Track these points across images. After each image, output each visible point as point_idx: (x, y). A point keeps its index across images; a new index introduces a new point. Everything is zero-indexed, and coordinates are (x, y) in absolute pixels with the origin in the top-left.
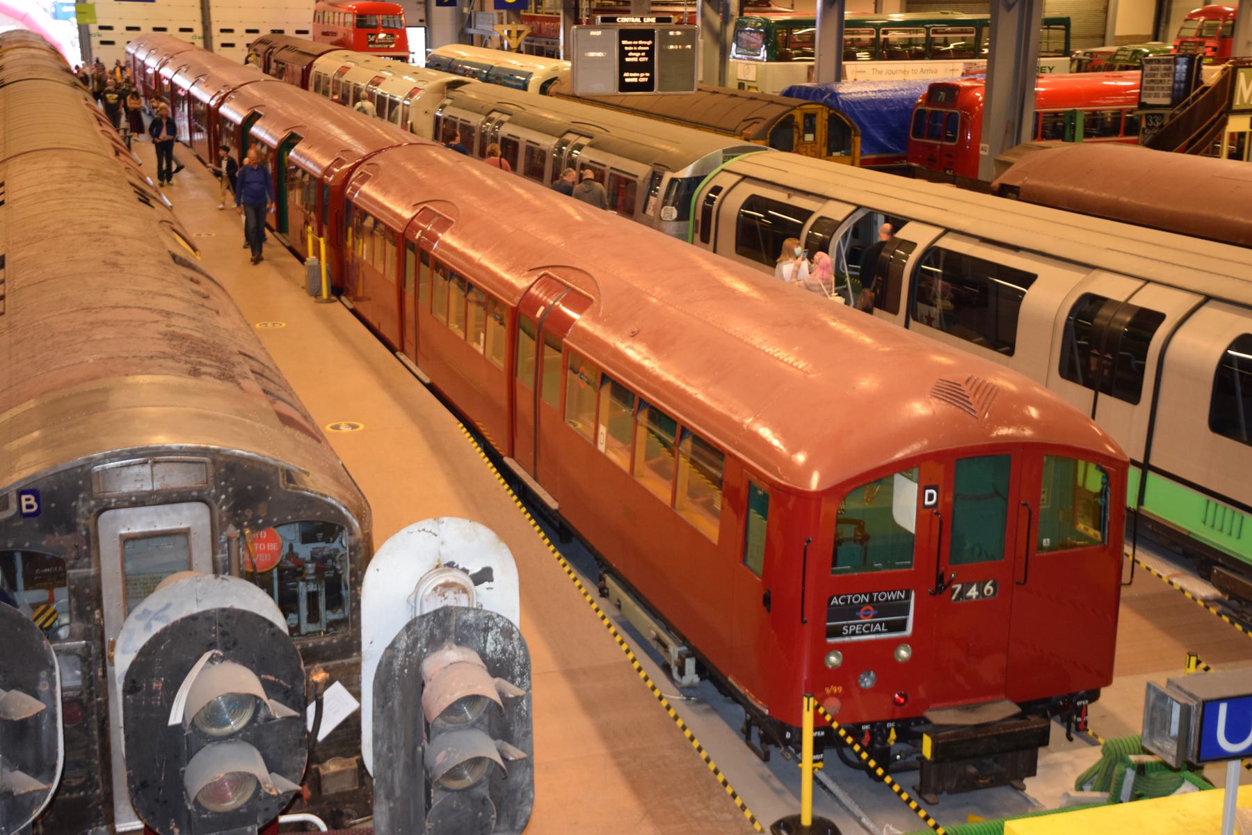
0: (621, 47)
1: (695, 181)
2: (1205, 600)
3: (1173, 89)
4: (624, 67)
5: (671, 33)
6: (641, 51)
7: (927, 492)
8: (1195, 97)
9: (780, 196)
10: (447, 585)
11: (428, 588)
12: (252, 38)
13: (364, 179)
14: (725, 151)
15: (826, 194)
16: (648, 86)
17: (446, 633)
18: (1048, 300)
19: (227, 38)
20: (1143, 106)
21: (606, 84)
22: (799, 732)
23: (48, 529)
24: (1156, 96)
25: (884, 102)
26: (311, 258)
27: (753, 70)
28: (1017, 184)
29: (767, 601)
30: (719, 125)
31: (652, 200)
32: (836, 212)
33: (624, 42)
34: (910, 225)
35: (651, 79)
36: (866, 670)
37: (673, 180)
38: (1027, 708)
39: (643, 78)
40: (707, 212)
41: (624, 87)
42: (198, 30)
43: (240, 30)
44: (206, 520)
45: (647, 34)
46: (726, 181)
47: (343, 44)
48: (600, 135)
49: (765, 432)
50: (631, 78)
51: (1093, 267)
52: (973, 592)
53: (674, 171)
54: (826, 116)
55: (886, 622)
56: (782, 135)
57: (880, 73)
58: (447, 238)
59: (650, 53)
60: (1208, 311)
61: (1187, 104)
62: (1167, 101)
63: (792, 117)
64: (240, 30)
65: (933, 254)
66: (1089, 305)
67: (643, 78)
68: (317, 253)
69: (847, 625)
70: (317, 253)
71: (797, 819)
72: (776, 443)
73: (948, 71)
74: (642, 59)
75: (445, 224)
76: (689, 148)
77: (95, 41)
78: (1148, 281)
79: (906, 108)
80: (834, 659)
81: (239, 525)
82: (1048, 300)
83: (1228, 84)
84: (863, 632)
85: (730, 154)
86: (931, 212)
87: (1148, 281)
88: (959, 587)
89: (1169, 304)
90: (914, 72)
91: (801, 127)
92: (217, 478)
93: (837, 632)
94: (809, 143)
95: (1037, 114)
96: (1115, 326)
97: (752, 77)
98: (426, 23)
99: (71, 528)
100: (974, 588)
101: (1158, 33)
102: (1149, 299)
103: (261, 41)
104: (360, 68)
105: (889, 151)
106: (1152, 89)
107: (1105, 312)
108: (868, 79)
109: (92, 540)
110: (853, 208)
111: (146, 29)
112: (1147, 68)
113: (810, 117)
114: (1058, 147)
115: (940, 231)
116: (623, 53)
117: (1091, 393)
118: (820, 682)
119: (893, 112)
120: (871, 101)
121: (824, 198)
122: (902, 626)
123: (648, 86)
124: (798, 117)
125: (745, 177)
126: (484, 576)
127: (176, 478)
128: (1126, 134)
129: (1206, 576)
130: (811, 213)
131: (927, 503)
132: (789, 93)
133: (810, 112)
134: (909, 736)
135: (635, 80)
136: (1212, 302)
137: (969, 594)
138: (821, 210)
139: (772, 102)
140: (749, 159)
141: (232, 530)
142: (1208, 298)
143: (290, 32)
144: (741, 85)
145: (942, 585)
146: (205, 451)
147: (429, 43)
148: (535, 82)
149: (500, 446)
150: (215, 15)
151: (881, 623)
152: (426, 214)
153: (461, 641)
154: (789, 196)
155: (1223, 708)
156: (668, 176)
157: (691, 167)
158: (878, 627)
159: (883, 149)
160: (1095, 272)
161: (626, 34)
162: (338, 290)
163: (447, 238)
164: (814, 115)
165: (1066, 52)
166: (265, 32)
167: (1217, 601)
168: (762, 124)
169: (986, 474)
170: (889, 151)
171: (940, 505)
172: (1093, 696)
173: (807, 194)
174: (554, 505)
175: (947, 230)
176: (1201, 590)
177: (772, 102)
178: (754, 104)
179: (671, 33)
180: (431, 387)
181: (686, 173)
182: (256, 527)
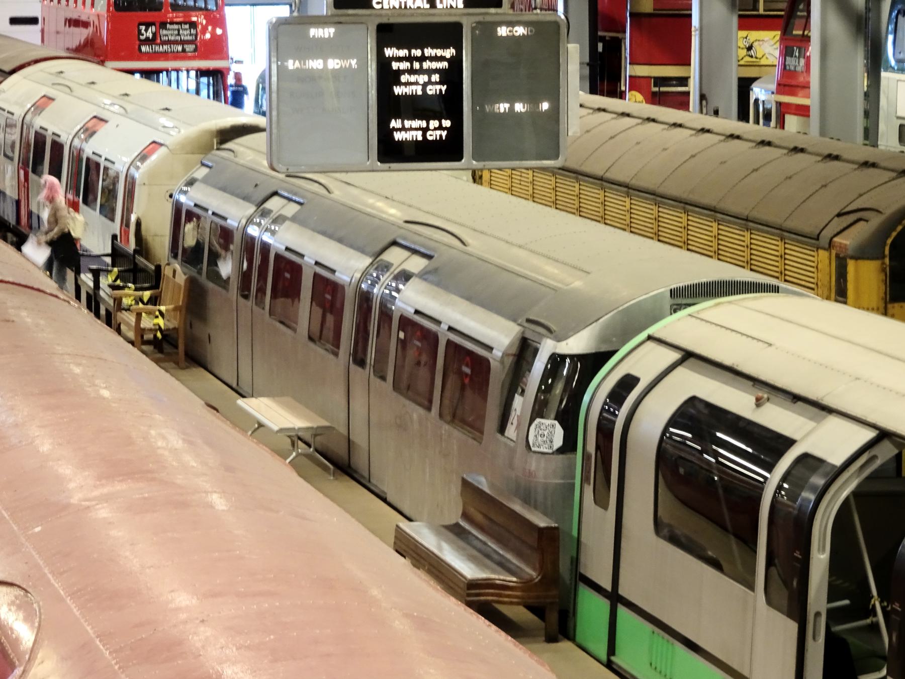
0: (384, 64)
1: (592, 363)
4: (390, 106)
5: (503, 31)
6: (430, 72)
14: (673, 293)
30: (789, 224)
32: (835, 442)
33: (389, 52)
37: (556, 361)
40: (605, 430)
46: (645, 361)
50: (408, 130)
53: (559, 339)
60: (680, 371)
74: (431, 90)
116: (387, 76)
125: (688, 356)
135: (419, 136)
154: (759, 403)
156: (547, 348)
168: (875, 221)
179: (503, 31)
181: (578, 343)
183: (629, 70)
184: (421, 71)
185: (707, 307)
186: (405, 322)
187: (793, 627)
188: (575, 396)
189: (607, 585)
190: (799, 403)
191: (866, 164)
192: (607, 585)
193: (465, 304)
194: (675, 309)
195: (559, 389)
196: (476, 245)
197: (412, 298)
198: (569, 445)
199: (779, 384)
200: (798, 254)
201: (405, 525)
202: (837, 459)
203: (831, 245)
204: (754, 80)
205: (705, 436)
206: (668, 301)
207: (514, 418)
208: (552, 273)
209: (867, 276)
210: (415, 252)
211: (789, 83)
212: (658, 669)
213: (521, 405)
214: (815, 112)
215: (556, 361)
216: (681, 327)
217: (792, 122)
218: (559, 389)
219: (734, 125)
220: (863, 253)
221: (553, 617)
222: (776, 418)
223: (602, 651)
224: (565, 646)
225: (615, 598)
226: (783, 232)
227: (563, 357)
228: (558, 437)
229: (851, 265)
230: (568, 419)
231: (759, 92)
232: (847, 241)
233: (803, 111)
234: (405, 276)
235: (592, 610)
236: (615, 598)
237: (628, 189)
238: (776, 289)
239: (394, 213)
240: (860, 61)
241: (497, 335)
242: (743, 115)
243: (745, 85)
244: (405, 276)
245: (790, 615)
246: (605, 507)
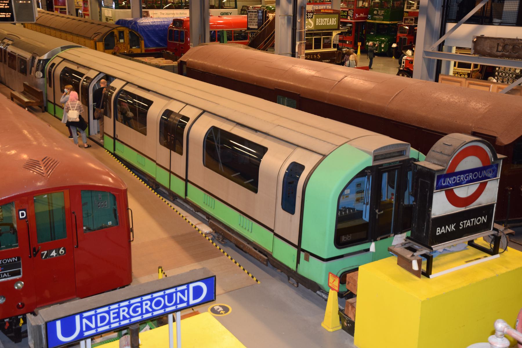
1: (47, 61)
2: (206, 234)
3: (258, 22)
6: (5, 3)
7: (20, 212)
8: (265, 25)
14: (61, 48)
15: (91, 67)
20: (249, 29)
24: (253, 25)
25: (157, 26)
27: (110, 12)
28: (185, 60)
30: (86, 36)
31: (33, 69)
32: (92, 74)
34: (116, 80)
35: (12, 15)
36: (18, 291)
37: (39, 61)
39: (8, 15)
40: (50, 73)
46: (57, 61)
49: (92, 166)
51: (172, 98)
52: (54, 254)
53: (40, 56)
54: (128, 32)
55: (9, 272)
57: (164, 14)
60: (63, 62)
61: (263, 27)
62: (256, 27)
63: (113, 33)
66: (168, 113)
67: (8, 15)
72: (97, 168)
73: (183, 14)
78: (187, 104)
79: (166, 29)
85: (63, 48)
87: (187, 104)
88: (46, 252)
89: (190, 113)
90: (177, 14)
91: (118, 36)
94: (121, 43)
95: (211, 31)
96: (175, 121)
97: (110, 15)
100: (54, 251)
105: (161, 46)
106: (251, 22)
110: (98, 73)
112: (249, 14)
114: (217, 45)
115: (125, 83)
117: (169, 150)
119: (161, 30)
121: (89, 68)
124: (116, 32)
125: (64, 59)
128: (234, 40)
131: (21, 217)
133: (121, 30)
135: (4, 16)
136: (206, 113)
137: (52, 254)
139: (106, 26)
140: (68, 52)
142: (204, 111)
144: (107, 19)
145: (36, 252)
151: (6, 273)
154: (78, 68)
155: (58, 324)
156: (38, 58)
157: (46, 55)
158: (5, 275)
159: (158, 45)
160: (172, 100)
164: (123, 32)
165: (236, 8)
167: (210, 233)
168: (101, 35)
170: (161, 46)
171: (28, 217)
173: (84, 67)
175: (128, 83)
176: (205, 229)
177: (106, 26)
181: (45, 57)
183: (54, 7)
184: (3, 3)
185: (67, 50)
186: (9, 53)
187: (87, 107)
188: (44, 68)
189: (53, 102)
190: (259, 133)
191: (99, 24)
192: (53, 102)
193: (21, 50)
194: (62, 51)
195: (41, 66)
196: (22, 38)
197: (10, 49)
198: (43, 77)
199: (82, 64)
200: (87, 41)
201: (13, 92)
202: (92, 77)
203: (93, 39)
204: (78, 9)
205: (168, 117)
206: (60, 49)
207: (32, 71)
208: (38, 44)
209: (100, 45)
210: (10, 40)
211: (85, 9)
212: (244, 227)
213: (34, 69)
214: (90, 15)
215: (39, 61)
216: (63, 54)
217: (87, 17)
218: (41, 66)
219: (74, 17)
220: (99, 41)
221: (43, 108)
222: (81, 70)
223: (53, 113)
224: (46, 113)
225: (55, 104)
226: (85, 37)
227: (41, 60)
228: (41, 75)
229: (97, 43)
230: (43, 71)
231: (80, 11)
232: (96, 38)
233: (88, 15)
234: (8, 45)
235: (51, 106)
236: (55, 104)
237: (54, 29)
238: (81, 47)
239: (6, 32)
240: (97, 6)
241: (28, 56)
242: (77, 16)
243: (77, 10)
244: (8, 45)
245: (86, 105)
246: (292, 212)
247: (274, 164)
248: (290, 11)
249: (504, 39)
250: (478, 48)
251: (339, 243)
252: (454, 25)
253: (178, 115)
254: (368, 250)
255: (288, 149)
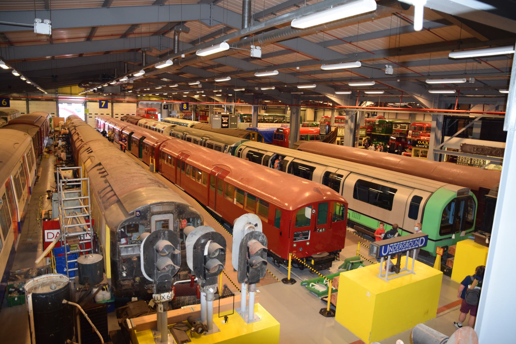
1: (235, 148)
4: (223, 123)
9: (256, 151)
10: (250, 227)
11: (247, 228)
12: (122, 116)
13: (164, 146)
16: (228, 127)
17: (252, 237)
18: (319, 172)
19: (117, 116)
20: (320, 134)
21: (218, 126)
22: (288, 261)
23: (141, 219)
25: (268, 132)
26: (151, 164)
29: (281, 234)
32: (270, 154)
38: (330, 253)
39: (226, 125)
41: (222, 127)
42: (111, 114)
43: (93, 114)
44: (172, 217)
45: (227, 116)
46: (243, 147)
47: (143, 117)
48: (211, 137)
50: (224, 125)
52: (321, 231)
56: (248, 137)
58: (188, 159)
59: (228, 120)
60: (351, 175)
64: (120, 114)
65: (293, 163)
66: (327, 174)
67: (226, 125)
68: (152, 162)
69: (297, 238)
70: (152, 162)
71: (287, 278)
75: (188, 156)
76: (234, 141)
77: (88, 117)
80: (295, 245)
81: (179, 219)
82: (319, 172)
83: (336, 130)
84: (300, 240)
85: (242, 142)
86: (291, 155)
89: (344, 173)
92: (175, 208)
93: (295, 240)
98: (161, 113)
99: (146, 219)
101: (315, 120)
102: (340, 172)
103: (125, 117)
104: (151, 123)
107: (331, 175)
108: (263, 127)
109: (150, 222)
111: (99, 114)
113: (254, 134)
116: (222, 120)
118: (292, 250)
120: (265, 131)
121: (266, 151)
122: (307, 238)
123: (228, 127)
124: (251, 134)
125: (247, 147)
126: (256, 225)
127: (167, 208)
129: (353, 228)
130: (264, 154)
132: (248, 129)
134: (308, 261)
138: (266, 154)
141: (178, 220)
142: (351, 172)
143: (131, 114)
145: (315, 230)
146: (173, 203)
147: (161, 117)
148: (189, 125)
149: (204, 204)
150: (114, 111)
152: (182, 154)
153: (255, 238)
161: (223, 116)
162: (157, 171)
163: (188, 159)
166: (125, 115)
167: (355, 232)
169: (320, 206)
172: (340, 251)
174: (221, 216)
175: (295, 158)
178: (241, 131)
180: (184, 191)
181: (233, 145)
182: (183, 219)
246: (415, 218)
247: (402, 197)
248: (353, 126)
249: (477, 146)
250: (463, 149)
251: (441, 234)
252: (449, 137)
253: (335, 174)
254: (451, 238)
255: (411, 190)
